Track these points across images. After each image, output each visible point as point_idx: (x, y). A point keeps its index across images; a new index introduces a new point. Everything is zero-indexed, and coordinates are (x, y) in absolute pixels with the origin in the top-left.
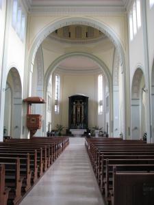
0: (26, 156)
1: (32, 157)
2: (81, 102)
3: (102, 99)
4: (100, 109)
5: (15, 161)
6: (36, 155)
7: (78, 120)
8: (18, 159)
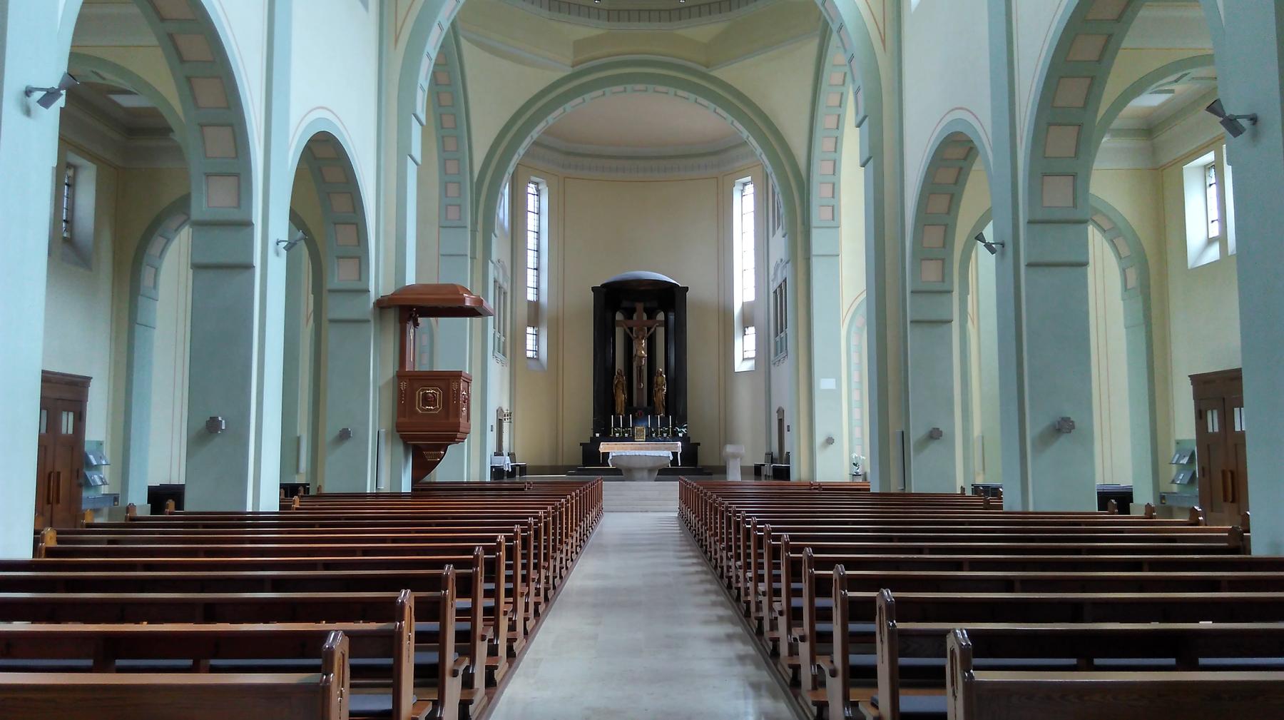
1: (466, 587)
2: (651, 314)
3: (750, 296)
4: (745, 348)
5: (391, 611)
7: (640, 398)
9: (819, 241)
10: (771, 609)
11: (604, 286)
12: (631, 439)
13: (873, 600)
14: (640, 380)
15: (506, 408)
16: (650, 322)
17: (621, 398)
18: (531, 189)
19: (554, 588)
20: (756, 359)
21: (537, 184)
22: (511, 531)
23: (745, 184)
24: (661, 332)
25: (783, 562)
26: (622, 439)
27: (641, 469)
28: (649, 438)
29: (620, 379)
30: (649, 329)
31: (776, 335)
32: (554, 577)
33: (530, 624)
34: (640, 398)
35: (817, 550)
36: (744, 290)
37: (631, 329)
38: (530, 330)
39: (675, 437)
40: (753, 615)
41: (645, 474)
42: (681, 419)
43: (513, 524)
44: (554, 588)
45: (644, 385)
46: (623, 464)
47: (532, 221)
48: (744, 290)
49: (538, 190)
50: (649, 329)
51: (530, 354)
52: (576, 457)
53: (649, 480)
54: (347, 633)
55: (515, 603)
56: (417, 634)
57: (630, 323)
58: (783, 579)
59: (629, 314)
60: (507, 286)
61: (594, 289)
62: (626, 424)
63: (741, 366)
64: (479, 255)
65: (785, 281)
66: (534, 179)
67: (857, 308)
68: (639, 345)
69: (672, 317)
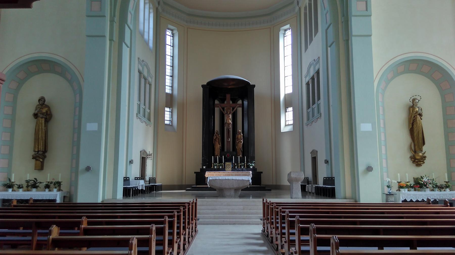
0: (163, 223)
1: (160, 232)
2: (234, 101)
3: (289, 90)
4: (287, 119)
5: (148, 231)
6: (167, 226)
7: (228, 146)
8: (154, 227)
9: (356, 26)
10: (281, 241)
11: (209, 83)
12: (223, 169)
13: (308, 228)
14: (228, 137)
15: (149, 150)
16: (234, 105)
17: (218, 146)
18: (169, 33)
19: (192, 236)
20: (293, 124)
21: (172, 30)
22: (179, 209)
23: (286, 30)
24: (240, 110)
25: (286, 221)
26: (218, 170)
27: (230, 189)
28: (233, 169)
29: (217, 136)
30: (233, 109)
31: (308, 107)
32: (192, 232)
33: (190, 239)
34: (228, 146)
35: (301, 217)
36: (286, 86)
37: (223, 109)
38: (167, 109)
39: (248, 168)
40: (269, 236)
41: (232, 192)
42: (252, 159)
43: (179, 206)
44: (192, 236)
45: (231, 140)
46: (217, 185)
47: (169, 50)
48: (286, 86)
49: (173, 34)
50: (233, 109)
51: (167, 122)
52: (191, 179)
53: (235, 197)
54: (136, 238)
55: (180, 238)
56: (138, 252)
57: (223, 105)
58: (286, 228)
59: (222, 101)
60: (152, 80)
61: (203, 86)
62: (221, 161)
63: (284, 129)
64: (116, 38)
65: (318, 73)
66: (170, 26)
67: (382, 75)
68: (227, 113)
69: (246, 103)
